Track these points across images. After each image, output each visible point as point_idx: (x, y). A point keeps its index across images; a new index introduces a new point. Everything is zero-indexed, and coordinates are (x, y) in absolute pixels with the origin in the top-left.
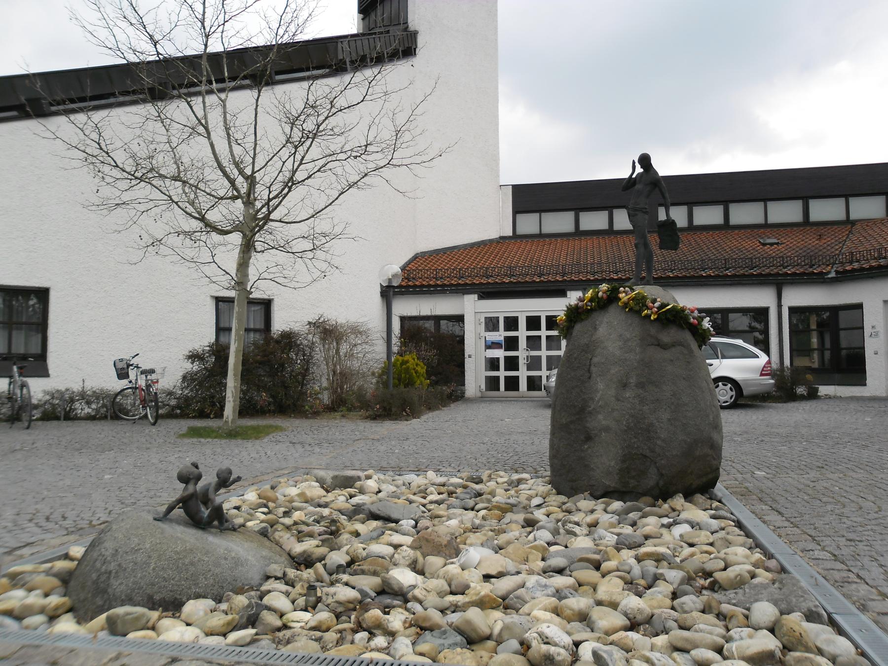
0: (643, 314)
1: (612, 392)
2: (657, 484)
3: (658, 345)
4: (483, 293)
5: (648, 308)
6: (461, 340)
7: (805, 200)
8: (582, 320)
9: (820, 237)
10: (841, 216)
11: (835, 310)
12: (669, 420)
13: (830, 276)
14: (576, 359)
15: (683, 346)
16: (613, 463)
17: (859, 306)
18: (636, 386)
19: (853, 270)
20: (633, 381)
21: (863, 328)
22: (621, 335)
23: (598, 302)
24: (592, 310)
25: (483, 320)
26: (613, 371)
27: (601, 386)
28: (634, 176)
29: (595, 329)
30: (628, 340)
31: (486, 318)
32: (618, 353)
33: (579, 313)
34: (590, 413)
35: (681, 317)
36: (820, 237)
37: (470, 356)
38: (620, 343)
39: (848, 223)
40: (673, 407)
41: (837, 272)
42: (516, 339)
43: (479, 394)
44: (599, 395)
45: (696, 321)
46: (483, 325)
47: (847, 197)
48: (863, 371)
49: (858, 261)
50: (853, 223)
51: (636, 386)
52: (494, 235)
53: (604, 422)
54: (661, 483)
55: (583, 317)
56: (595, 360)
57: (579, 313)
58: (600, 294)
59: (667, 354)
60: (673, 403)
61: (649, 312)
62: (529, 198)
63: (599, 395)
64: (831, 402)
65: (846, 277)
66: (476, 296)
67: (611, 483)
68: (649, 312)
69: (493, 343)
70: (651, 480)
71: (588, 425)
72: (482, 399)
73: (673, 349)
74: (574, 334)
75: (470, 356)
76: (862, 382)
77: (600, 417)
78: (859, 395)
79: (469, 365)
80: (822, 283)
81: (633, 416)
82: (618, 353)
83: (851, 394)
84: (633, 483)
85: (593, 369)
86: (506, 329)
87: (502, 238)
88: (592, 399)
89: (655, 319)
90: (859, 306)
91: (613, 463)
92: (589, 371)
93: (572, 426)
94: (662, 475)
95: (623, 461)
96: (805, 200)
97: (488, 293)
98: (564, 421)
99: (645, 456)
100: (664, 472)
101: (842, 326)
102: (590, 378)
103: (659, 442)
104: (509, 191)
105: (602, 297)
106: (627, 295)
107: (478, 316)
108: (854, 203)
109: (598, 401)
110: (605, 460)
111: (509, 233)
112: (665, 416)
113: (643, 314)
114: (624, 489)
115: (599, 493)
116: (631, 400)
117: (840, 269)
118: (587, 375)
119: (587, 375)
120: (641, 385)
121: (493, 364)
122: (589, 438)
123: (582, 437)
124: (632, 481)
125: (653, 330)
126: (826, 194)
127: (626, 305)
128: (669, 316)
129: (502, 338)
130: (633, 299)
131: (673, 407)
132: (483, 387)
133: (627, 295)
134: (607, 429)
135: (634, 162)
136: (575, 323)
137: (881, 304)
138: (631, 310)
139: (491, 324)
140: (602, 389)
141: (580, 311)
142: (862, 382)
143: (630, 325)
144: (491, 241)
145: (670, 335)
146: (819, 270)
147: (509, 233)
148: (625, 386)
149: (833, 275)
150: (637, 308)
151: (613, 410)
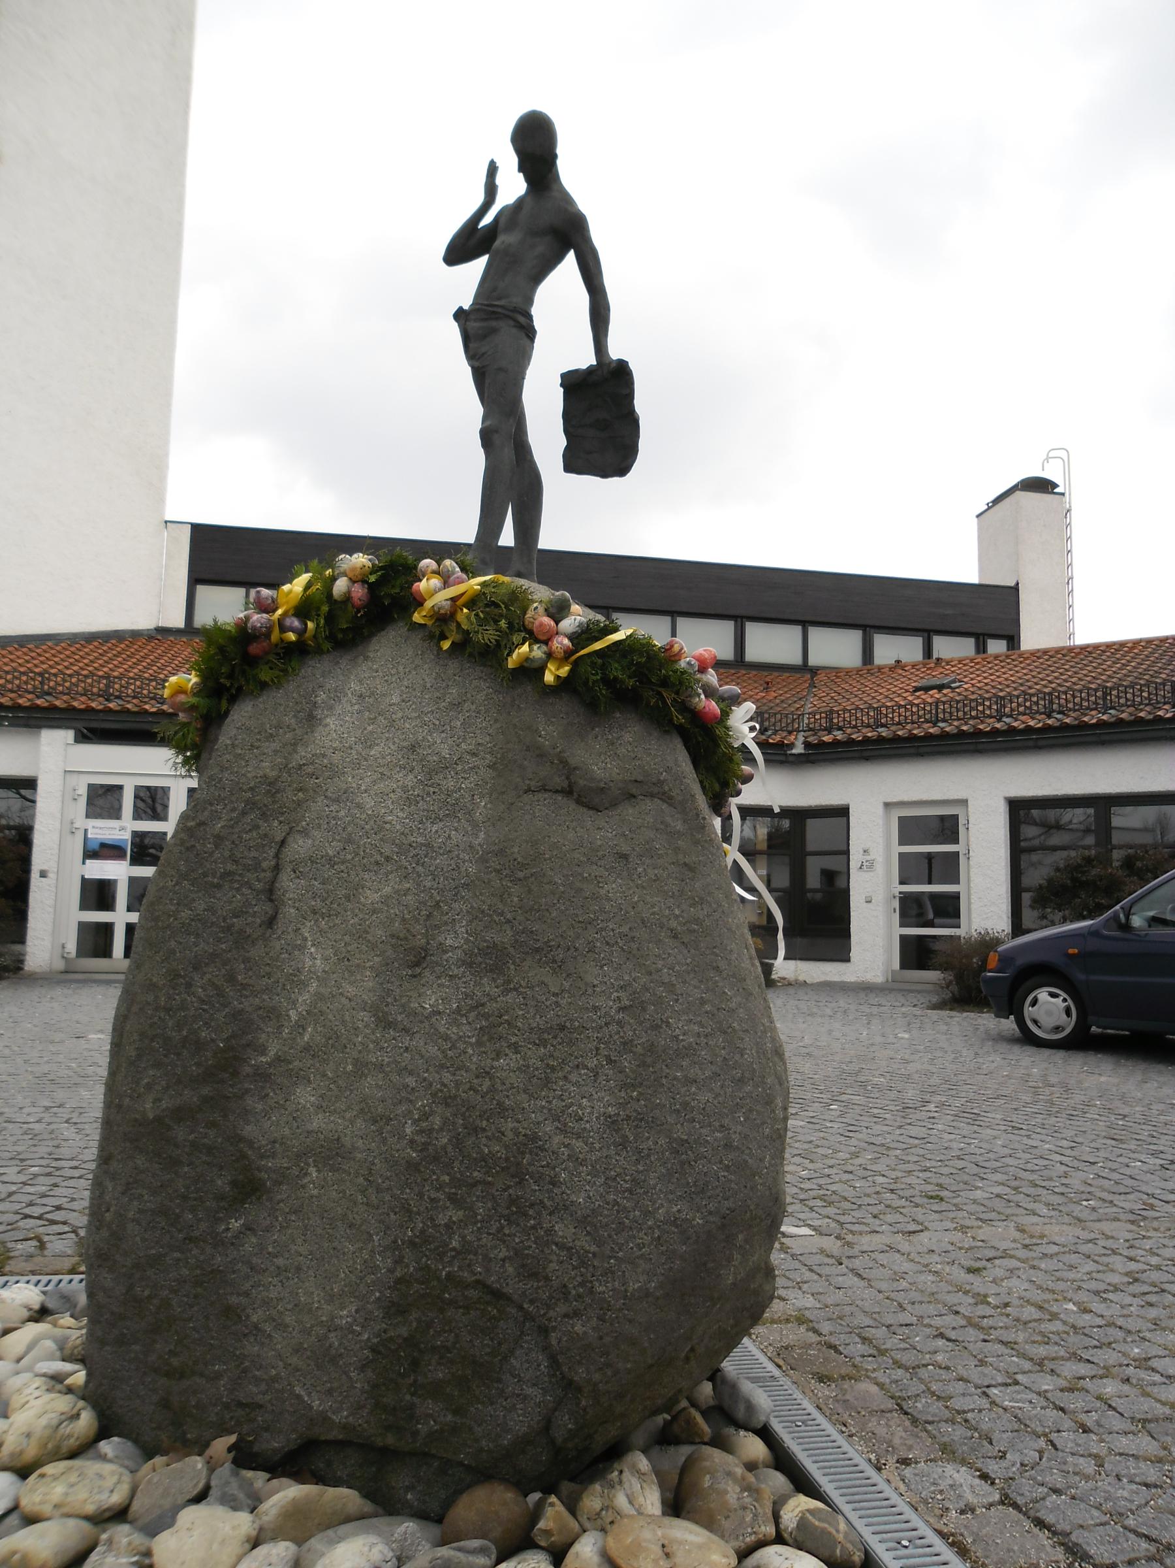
0: (513, 661)
1: (362, 987)
2: (547, 1426)
3: (568, 792)
4: (90, 730)
5: (533, 637)
6: (23, 836)
7: (740, 620)
8: (264, 686)
9: (767, 686)
10: (795, 658)
11: (798, 816)
12: (612, 1123)
13: (794, 751)
14: (219, 839)
15: (667, 798)
16: (345, 1315)
17: (843, 812)
18: (468, 963)
19: (836, 743)
20: (454, 939)
21: (847, 853)
22: (413, 748)
23: (330, 618)
24: (299, 651)
25: (83, 791)
26: (371, 897)
27: (315, 959)
28: (488, 219)
29: (311, 720)
30: (444, 766)
31: (91, 787)
32: (397, 818)
33: (251, 661)
34: (262, 1076)
35: (665, 682)
36: (767, 686)
37: (43, 874)
38: (410, 780)
39: (805, 669)
40: (627, 1062)
41: (807, 745)
42: (115, 813)
43: (60, 965)
44: (304, 999)
45: (713, 706)
46: (83, 801)
47: (805, 624)
48: (846, 934)
49: (840, 729)
50: (814, 671)
51: (468, 963)
52: (142, 619)
53: (317, 1122)
54: (565, 1423)
55: (265, 675)
56: (299, 847)
57: (251, 661)
58: (341, 586)
59: (602, 831)
60: (627, 1045)
61: (538, 652)
62: (221, 553)
63: (304, 999)
64: (791, 990)
65: (825, 753)
66: (69, 735)
67: (332, 1402)
68: (538, 652)
69: (103, 845)
70: (518, 1408)
71: (249, 1130)
72: (67, 975)
73: (629, 812)
74: (224, 739)
75: (43, 874)
76: (843, 956)
77: (305, 1096)
78: (836, 979)
79: (40, 895)
80: (782, 763)
81: (447, 1102)
82: (397, 818)
83: (822, 978)
84: (432, 1416)
85: (288, 884)
86: (138, 815)
87: (163, 631)
88: (274, 1014)
89: (563, 684)
90: (843, 812)
91: (345, 1315)
92: (271, 892)
93: (180, 1133)
94: (569, 1385)
95: (396, 1310)
96: (740, 620)
97: (99, 728)
98: (148, 1107)
99: (497, 1295)
100: (580, 1374)
101: (810, 847)
102: (271, 922)
103: (564, 1230)
104: (187, 532)
105: (347, 597)
106: (446, 584)
107: (73, 780)
108: (793, 656)
109: (300, 1027)
110: (313, 1294)
111: (179, 622)
112: (594, 1103)
113: (513, 661)
114: (390, 1440)
115: (274, 1444)
116: (442, 1025)
117: (813, 740)
118: (262, 908)
119: (262, 908)
120: (490, 960)
121: (98, 894)
122: (248, 1189)
123: (222, 1183)
124: (430, 1406)
125: (550, 728)
126: (773, 616)
127: (444, 619)
128: (616, 671)
129: (127, 836)
130: (473, 602)
131: (627, 1062)
132: (72, 948)
133: (446, 584)
134: (332, 1153)
135: (492, 169)
136: (233, 700)
137: (880, 809)
138: (462, 646)
139: (103, 799)
140: (321, 971)
141: (254, 649)
142: (843, 956)
143: (456, 706)
144: (135, 635)
145: (623, 751)
146: (778, 738)
147: (179, 622)
148: (418, 960)
149: (799, 749)
150: (488, 635)
151: (361, 1068)
